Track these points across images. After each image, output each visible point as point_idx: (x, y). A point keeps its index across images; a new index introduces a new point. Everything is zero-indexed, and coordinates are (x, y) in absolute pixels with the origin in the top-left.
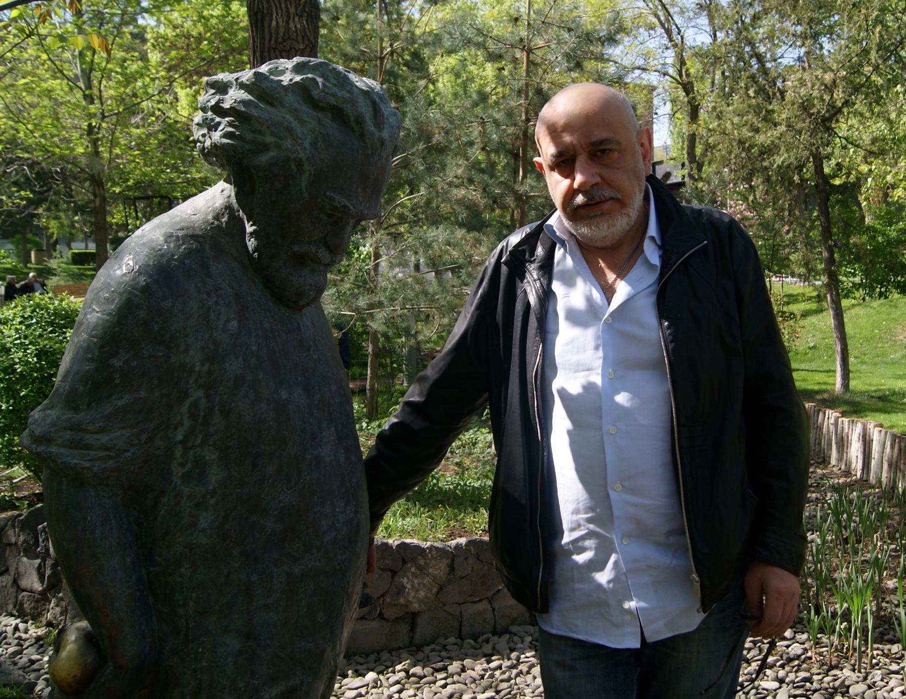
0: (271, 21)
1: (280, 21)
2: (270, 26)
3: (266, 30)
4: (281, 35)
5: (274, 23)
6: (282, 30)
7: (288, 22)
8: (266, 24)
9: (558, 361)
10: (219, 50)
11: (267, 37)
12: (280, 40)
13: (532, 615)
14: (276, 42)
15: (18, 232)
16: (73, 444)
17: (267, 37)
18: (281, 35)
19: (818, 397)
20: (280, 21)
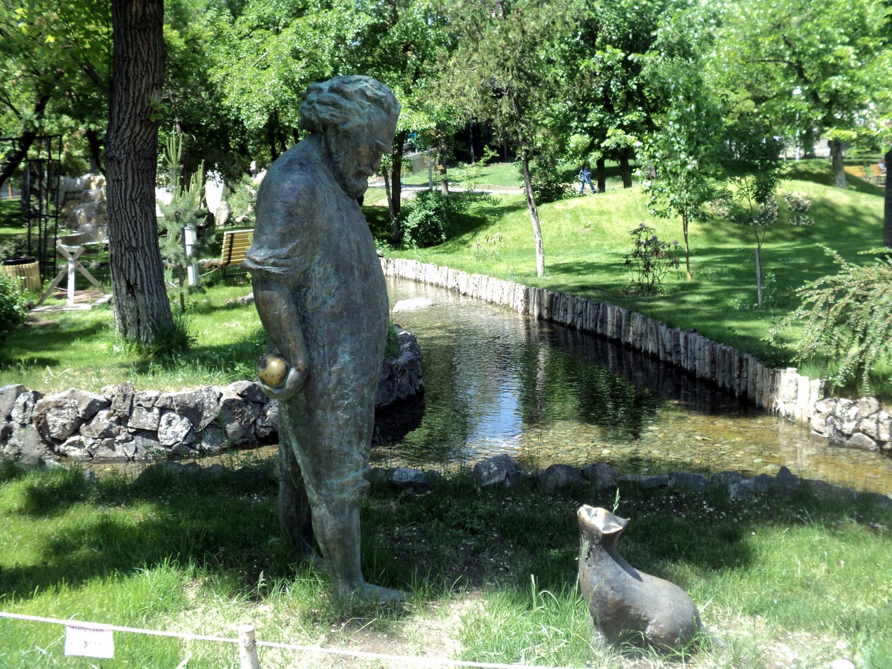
0: (131, 7)
1: (139, 6)
2: (131, 11)
3: (128, 14)
4: (139, 17)
5: (134, 9)
6: (140, 14)
7: (144, 8)
8: (128, 9)
9: (720, 423)
10: (118, 181)
11: (129, 18)
12: (139, 21)
13: (40, 139)
14: (136, 23)
15: (753, 170)
16: (274, 264)
17: (129, 18)
18: (139, 17)
19: (645, 311)
20: (139, 6)
